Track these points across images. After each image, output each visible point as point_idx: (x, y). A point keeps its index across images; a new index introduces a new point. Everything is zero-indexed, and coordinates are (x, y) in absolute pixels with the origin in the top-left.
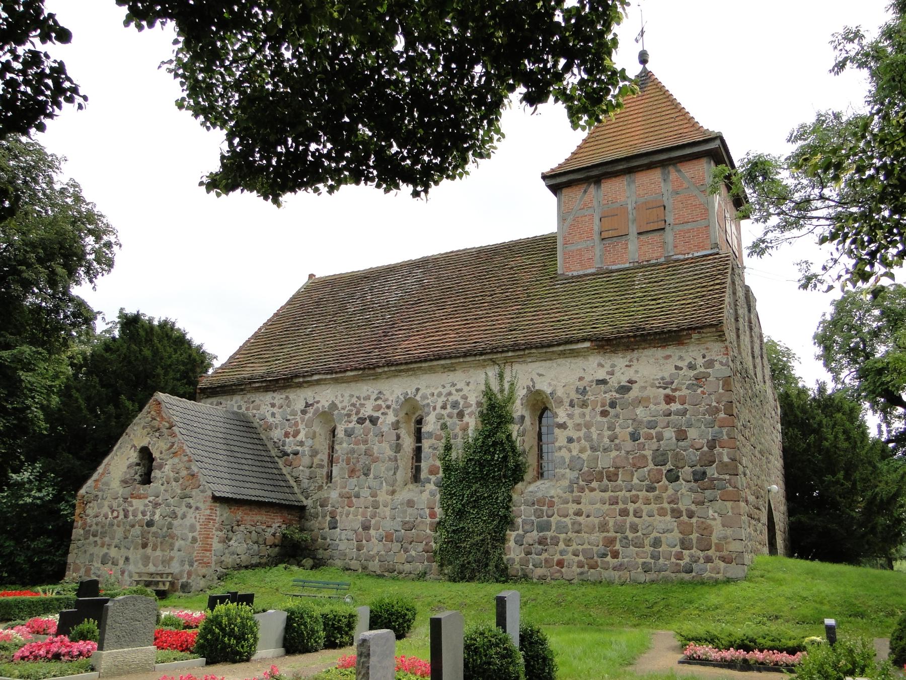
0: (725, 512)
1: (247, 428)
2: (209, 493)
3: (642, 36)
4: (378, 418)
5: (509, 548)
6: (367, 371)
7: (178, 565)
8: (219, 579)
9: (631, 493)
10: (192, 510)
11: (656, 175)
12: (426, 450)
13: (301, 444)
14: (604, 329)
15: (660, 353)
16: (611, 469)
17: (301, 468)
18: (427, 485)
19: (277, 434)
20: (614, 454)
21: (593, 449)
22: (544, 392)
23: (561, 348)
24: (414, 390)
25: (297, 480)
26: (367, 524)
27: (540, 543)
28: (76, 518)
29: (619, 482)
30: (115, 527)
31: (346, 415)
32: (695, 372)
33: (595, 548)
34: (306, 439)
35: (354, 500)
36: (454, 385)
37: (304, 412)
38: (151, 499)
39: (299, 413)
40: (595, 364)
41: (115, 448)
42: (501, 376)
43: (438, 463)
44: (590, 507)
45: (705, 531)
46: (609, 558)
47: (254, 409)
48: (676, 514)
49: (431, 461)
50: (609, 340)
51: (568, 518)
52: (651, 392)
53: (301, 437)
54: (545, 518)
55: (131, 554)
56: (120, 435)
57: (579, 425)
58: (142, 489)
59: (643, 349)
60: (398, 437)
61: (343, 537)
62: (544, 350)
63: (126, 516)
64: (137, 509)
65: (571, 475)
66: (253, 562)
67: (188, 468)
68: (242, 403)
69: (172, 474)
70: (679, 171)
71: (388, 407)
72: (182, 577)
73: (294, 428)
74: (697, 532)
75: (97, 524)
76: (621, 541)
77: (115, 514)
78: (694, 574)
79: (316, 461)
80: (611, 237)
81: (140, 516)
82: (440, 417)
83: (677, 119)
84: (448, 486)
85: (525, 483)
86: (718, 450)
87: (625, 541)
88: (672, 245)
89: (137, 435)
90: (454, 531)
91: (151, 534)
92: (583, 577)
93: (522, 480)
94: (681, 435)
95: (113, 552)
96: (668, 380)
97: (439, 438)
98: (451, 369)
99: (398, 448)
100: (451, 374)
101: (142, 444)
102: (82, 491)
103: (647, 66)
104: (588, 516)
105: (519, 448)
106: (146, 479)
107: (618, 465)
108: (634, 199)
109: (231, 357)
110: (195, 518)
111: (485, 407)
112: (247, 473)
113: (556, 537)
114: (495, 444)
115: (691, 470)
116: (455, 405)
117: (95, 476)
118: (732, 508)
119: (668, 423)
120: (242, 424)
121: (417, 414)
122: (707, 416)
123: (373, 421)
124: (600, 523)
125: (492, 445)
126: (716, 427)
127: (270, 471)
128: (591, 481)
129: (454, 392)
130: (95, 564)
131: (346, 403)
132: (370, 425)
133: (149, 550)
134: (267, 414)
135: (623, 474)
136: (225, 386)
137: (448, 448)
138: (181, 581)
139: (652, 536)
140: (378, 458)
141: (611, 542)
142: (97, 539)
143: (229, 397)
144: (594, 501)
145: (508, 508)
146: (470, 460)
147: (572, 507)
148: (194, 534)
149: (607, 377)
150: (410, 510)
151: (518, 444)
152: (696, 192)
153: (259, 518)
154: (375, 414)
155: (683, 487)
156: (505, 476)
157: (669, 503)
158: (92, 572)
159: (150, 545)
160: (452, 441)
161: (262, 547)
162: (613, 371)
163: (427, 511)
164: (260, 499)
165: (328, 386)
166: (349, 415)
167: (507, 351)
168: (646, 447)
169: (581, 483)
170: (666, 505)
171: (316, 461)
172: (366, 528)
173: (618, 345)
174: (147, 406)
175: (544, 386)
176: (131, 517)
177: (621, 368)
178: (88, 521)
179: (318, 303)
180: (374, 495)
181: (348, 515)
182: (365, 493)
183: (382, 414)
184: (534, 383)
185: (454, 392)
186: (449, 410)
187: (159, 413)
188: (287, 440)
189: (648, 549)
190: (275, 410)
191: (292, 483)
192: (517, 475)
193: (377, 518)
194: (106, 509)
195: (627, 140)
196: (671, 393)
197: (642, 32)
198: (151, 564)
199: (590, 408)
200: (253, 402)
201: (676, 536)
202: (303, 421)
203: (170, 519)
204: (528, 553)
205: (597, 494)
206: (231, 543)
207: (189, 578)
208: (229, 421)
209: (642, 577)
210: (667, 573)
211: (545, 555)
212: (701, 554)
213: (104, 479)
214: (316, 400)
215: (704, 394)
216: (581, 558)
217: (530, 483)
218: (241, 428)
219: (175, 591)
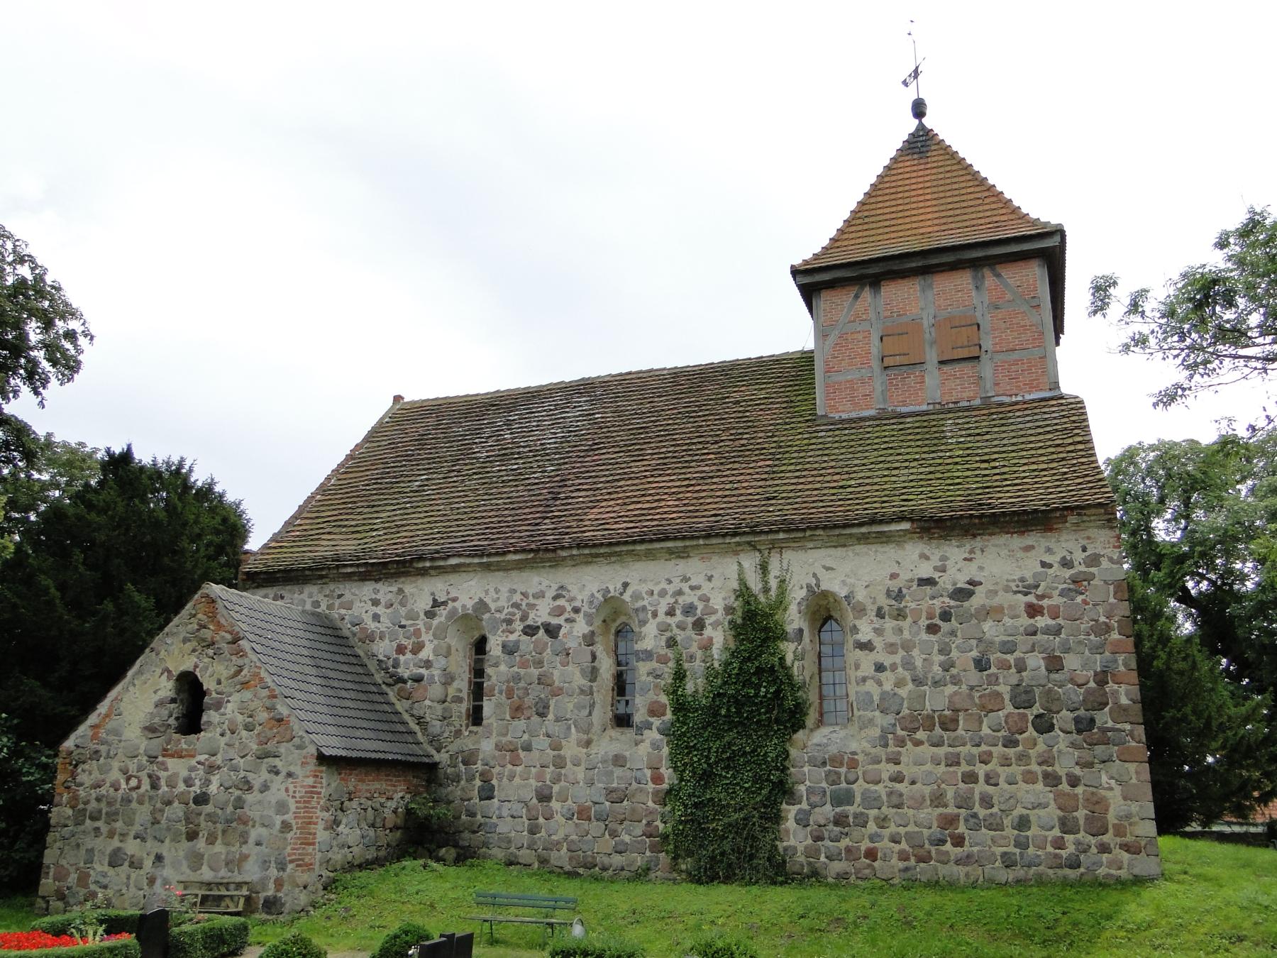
0: (1126, 778)
1: (336, 642)
2: (312, 750)
3: (916, 77)
4: (560, 627)
5: (787, 831)
7: (256, 868)
8: (325, 889)
9: (980, 749)
11: (964, 279)
12: (643, 678)
13: (428, 664)
14: (923, 503)
15: (1016, 541)
16: (946, 712)
17: (427, 702)
18: (646, 732)
19: (383, 648)
20: (950, 689)
21: (917, 681)
22: (833, 594)
23: (864, 530)
24: (619, 586)
25: (420, 720)
26: (546, 792)
27: (836, 823)
28: (60, 789)
29: (960, 732)
30: (134, 805)
31: (504, 621)
32: (1072, 571)
33: (925, 831)
34: (438, 660)
35: (522, 754)
36: (686, 579)
37: (430, 615)
38: (202, 758)
39: (422, 615)
40: (916, 556)
41: (130, 674)
42: (764, 568)
43: (664, 699)
44: (916, 769)
45: (1097, 805)
46: (948, 846)
47: (341, 606)
48: (1052, 780)
49: (649, 693)
50: (941, 520)
51: (881, 785)
52: (1003, 599)
53: (426, 653)
54: (844, 785)
55: (166, 849)
56: (141, 651)
57: (892, 645)
58: (184, 742)
59: (991, 534)
60: (594, 657)
61: (505, 813)
62: (837, 532)
63: (154, 786)
64: (176, 775)
65: (882, 720)
66: (369, 857)
67: (270, 709)
68: (320, 597)
69: (240, 718)
70: (998, 276)
71: (576, 610)
72: (264, 888)
73: (413, 639)
74: (1085, 807)
75: (98, 800)
76: (966, 820)
77: (134, 782)
78: (1082, 870)
79: (452, 691)
80: (899, 365)
81: (182, 787)
82: (664, 628)
83: (987, 201)
84: (684, 734)
85: (807, 731)
86: (1111, 687)
87: (973, 820)
88: (989, 381)
89: (171, 653)
90: (696, 805)
91: (198, 817)
92: (908, 875)
93: (803, 726)
94: (1054, 664)
95: (132, 847)
96: (1031, 581)
97: (663, 660)
98: (682, 554)
99: (593, 674)
100: (682, 563)
101: (182, 668)
102: (69, 744)
103: (924, 120)
104: (913, 783)
105: (798, 678)
106: (191, 723)
107: (958, 706)
108: (932, 311)
109: (287, 523)
110: (287, 790)
111: (740, 613)
112: (352, 713)
113: (862, 814)
114: (759, 671)
115: (1072, 715)
116: (689, 610)
117: (93, 719)
118: (1137, 773)
119: (1033, 646)
120: (329, 632)
121: (618, 622)
122: (1092, 637)
123: (552, 631)
124: (932, 793)
125: (754, 674)
126: (1107, 653)
127: (378, 707)
128: (915, 730)
129: (687, 590)
130: (98, 867)
131: (503, 602)
132: (546, 638)
133: (201, 844)
134: (364, 616)
135: (965, 720)
136: (292, 570)
137: (680, 676)
138: (262, 895)
139: (1016, 813)
140: (561, 689)
141: (950, 821)
142: (97, 824)
143: (296, 588)
144: (922, 761)
145: (784, 769)
146: (719, 695)
147: (887, 770)
148: (286, 817)
149: (936, 575)
150: (618, 772)
151: (795, 671)
152: (1025, 308)
153: (377, 785)
155: (1061, 741)
156: (777, 721)
157: (1039, 764)
159: (203, 835)
160: (686, 666)
161: (380, 832)
162: (944, 566)
163: (648, 773)
164: (382, 756)
165: (472, 575)
167: (777, 532)
168: (1001, 680)
169: (900, 732)
170: (1035, 767)
171: (452, 691)
172: (544, 797)
173: (953, 528)
174: (189, 606)
175: (834, 584)
176: (165, 788)
177: (956, 561)
178: (82, 793)
179: (421, 441)
180: (556, 747)
182: (541, 742)
183: (567, 620)
184: (818, 580)
185: (687, 590)
186: (679, 616)
187: (213, 616)
188: (402, 658)
189: (1010, 833)
190: (379, 610)
191: (413, 726)
192: (794, 719)
193: (562, 783)
194: (115, 775)
195: (914, 225)
196: (1035, 601)
197: (916, 73)
198: (205, 868)
199: (909, 620)
200: (340, 596)
201: (1053, 812)
202: (428, 628)
203: (239, 792)
204: (818, 838)
205: (926, 750)
206: (341, 828)
207: (278, 890)
208: (310, 628)
209: (1005, 875)
210: (1041, 868)
211: (845, 842)
212: (1093, 841)
213: (111, 725)
214: (452, 595)
215: (1087, 604)
216: (904, 845)
217: (812, 730)
218: (329, 639)
219: (253, 912)
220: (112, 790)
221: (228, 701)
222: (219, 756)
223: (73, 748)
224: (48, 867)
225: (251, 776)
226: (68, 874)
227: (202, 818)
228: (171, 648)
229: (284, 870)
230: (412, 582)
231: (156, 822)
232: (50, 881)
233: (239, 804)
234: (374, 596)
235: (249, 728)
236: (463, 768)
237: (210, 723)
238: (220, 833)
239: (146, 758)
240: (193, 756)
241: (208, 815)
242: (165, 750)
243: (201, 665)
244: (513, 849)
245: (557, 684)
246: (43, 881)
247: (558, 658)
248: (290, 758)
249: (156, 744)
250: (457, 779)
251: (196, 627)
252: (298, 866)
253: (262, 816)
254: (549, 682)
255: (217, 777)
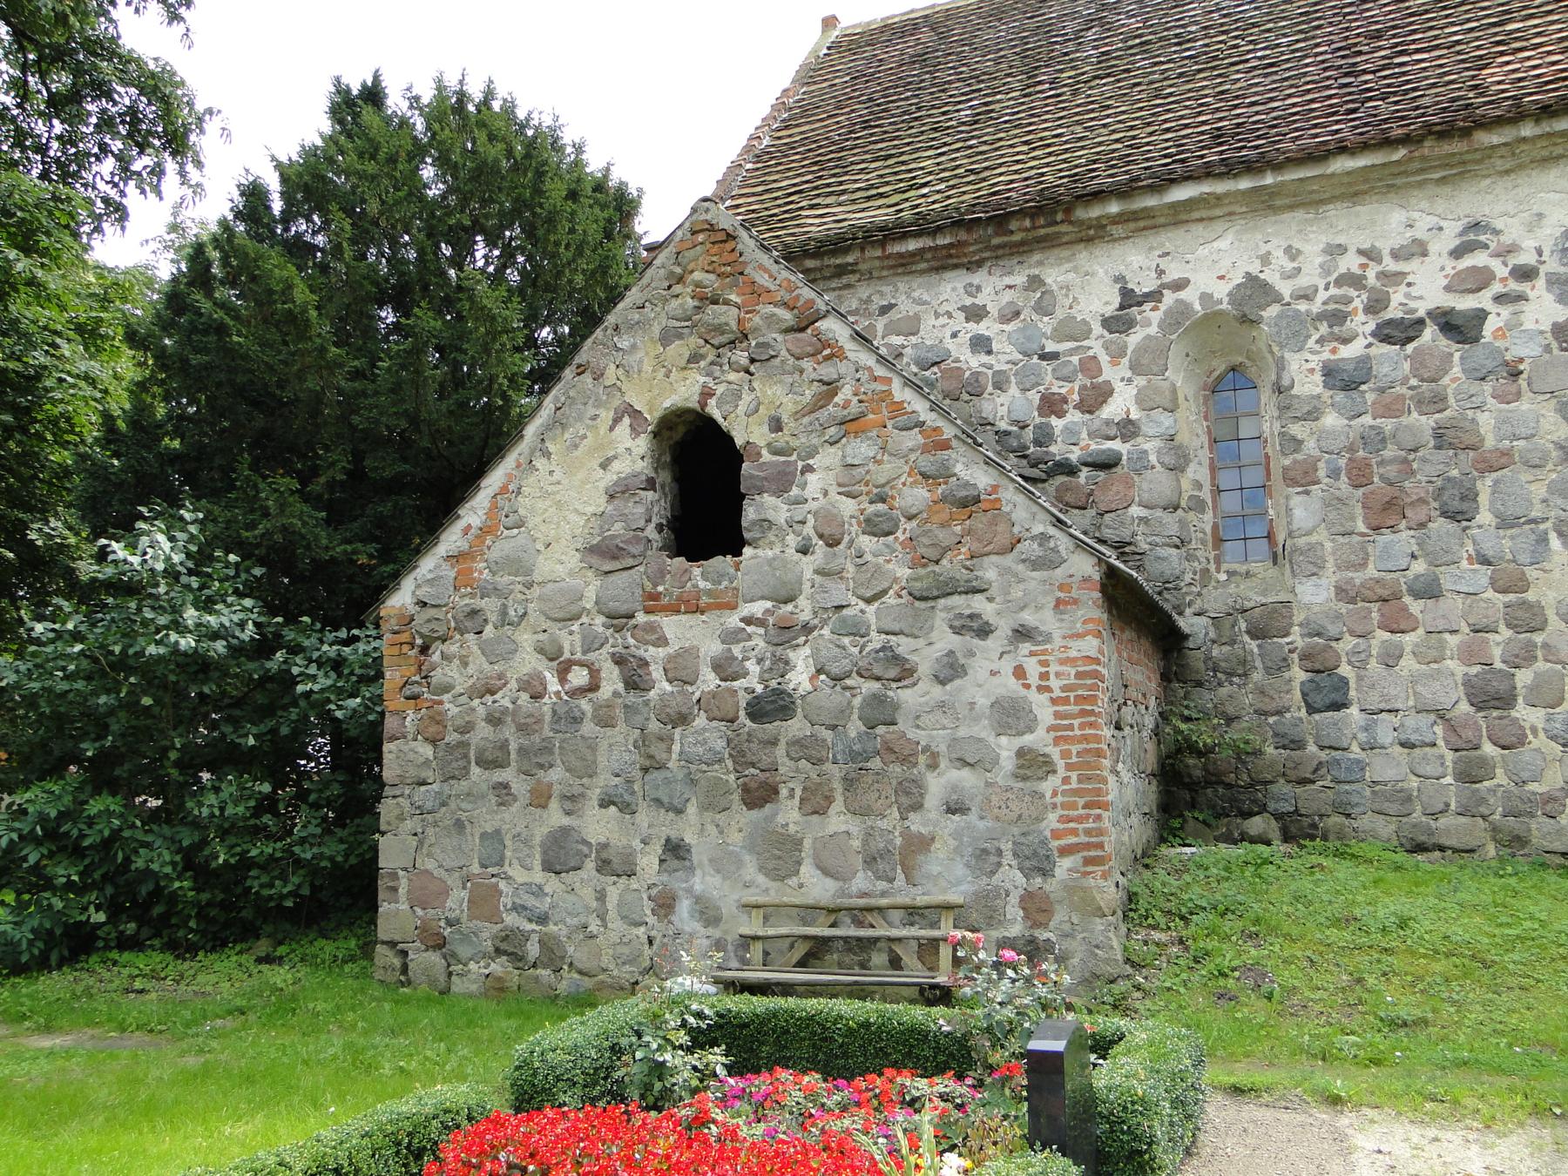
4: (1481, 316)
6: (1429, 147)
7: (960, 870)
10: (994, 644)
13: (1127, 429)
17: (1135, 511)
26: (1500, 686)
28: (394, 702)
30: (588, 728)
31: (1320, 317)
34: (1143, 407)
35: (1415, 606)
37: (1118, 324)
38: (758, 608)
39: (1097, 329)
41: (530, 431)
47: (891, 330)
58: (699, 576)
61: (1385, 735)
63: (635, 681)
64: (689, 653)
69: (848, 507)
71: (1525, 274)
77: (579, 677)
81: (709, 681)
95: (598, 825)
102: (401, 599)
110: (1019, 672)
117: (452, 539)
132: (1444, 343)
133: (788, 814)
134: (950, 344)
148: (1027, 739)
154: (1465, 303)
158: (507, 901)
165: (1219, 226)
166: (1337, 317)
172: (1492, 697)
181: (1391, 659)
182: (1466, 576)
183: (1499, 299)
193: (1541, 665)
194: (528, 661)
198: (807, 871)
200: (884, 310)
202: (1117, 354)
203: (876, 685)
213: (498, 550)
214: (1173, 274)
220: (524, 696)
221: (809, 469)
222: (802, 601)
223: (413, 609)
224: (394, 876)
225: (903, 645)
226: (446, 892)
227: (780, 751)
228: (631, 359)
229: (1046, 873)
230: (1060, 261)
231: (651, 766)
232: (404, 906)
233: (880, 713)
234: (968, 301)
235: (877, 527)
236: (1253, 645)
237: (766, 524)
238: (838, 786)
239: (600, 620)
240: (733, 607)
241: (796, 742)
242: (655, 597)
243: (720, 389)
244: (1417, 816)
245: (1490, 442)
246: (384, 908)
247: (1487, 387)
248: (1017, 593)
249: (625, 587)
250: (1240, 669)
251: (691, 303)
252: (1088, 861)
253: (954, 742)
254: (1468, 439)
255: (807, 651)
